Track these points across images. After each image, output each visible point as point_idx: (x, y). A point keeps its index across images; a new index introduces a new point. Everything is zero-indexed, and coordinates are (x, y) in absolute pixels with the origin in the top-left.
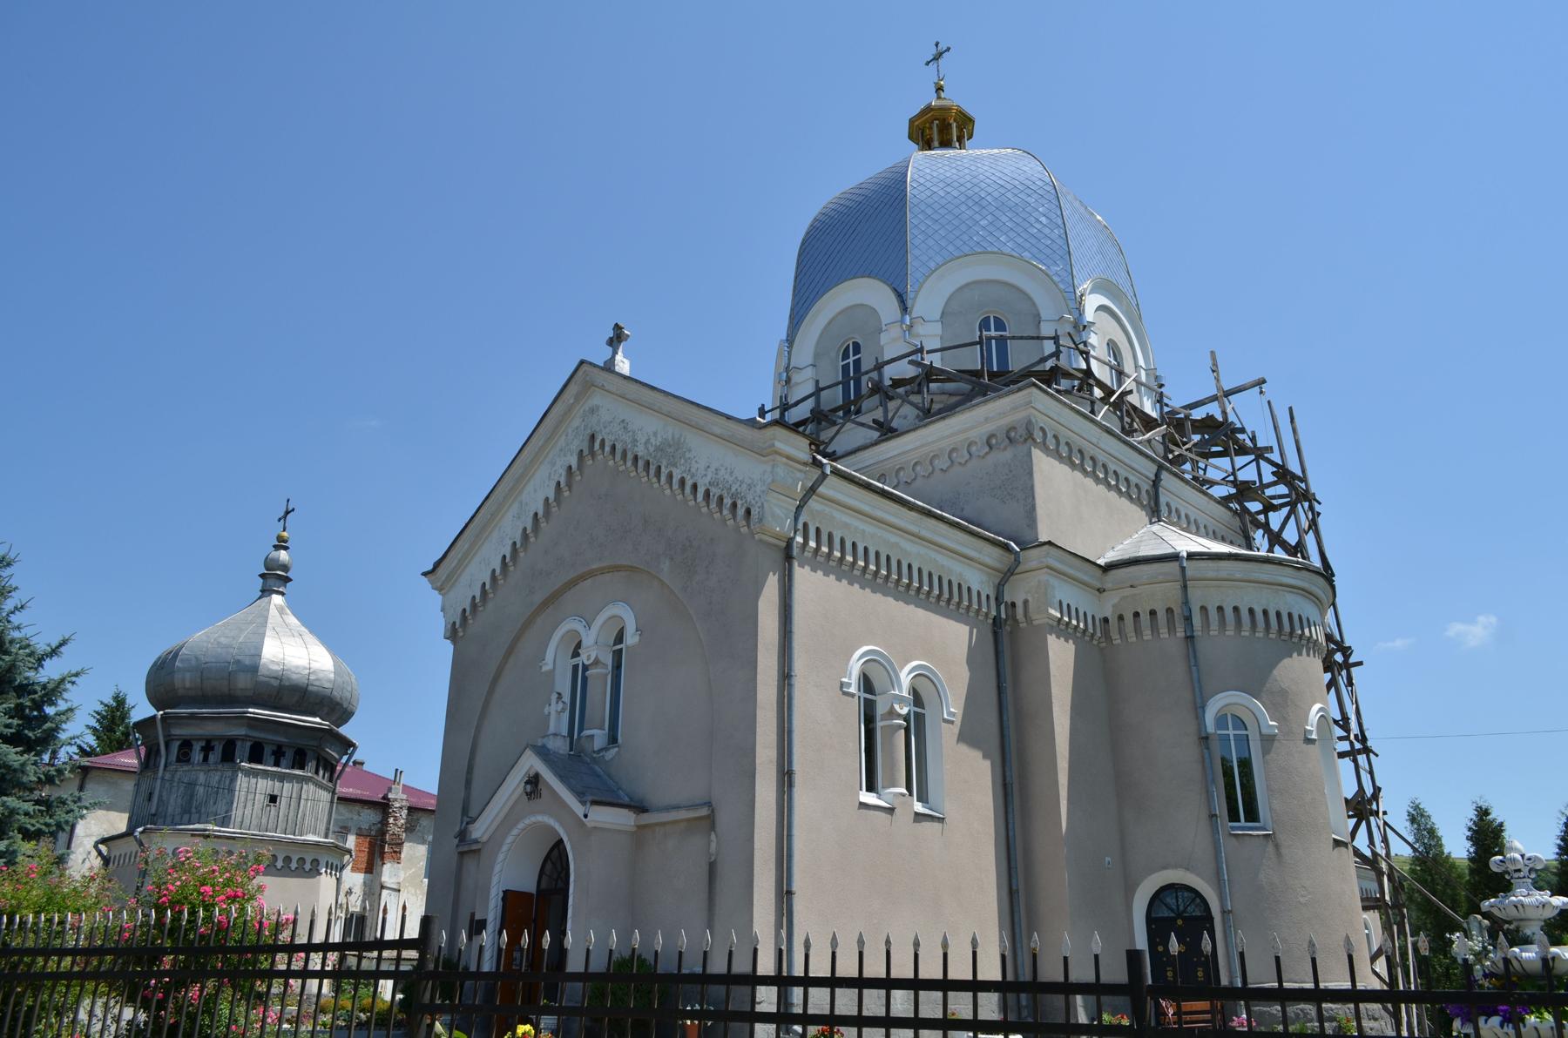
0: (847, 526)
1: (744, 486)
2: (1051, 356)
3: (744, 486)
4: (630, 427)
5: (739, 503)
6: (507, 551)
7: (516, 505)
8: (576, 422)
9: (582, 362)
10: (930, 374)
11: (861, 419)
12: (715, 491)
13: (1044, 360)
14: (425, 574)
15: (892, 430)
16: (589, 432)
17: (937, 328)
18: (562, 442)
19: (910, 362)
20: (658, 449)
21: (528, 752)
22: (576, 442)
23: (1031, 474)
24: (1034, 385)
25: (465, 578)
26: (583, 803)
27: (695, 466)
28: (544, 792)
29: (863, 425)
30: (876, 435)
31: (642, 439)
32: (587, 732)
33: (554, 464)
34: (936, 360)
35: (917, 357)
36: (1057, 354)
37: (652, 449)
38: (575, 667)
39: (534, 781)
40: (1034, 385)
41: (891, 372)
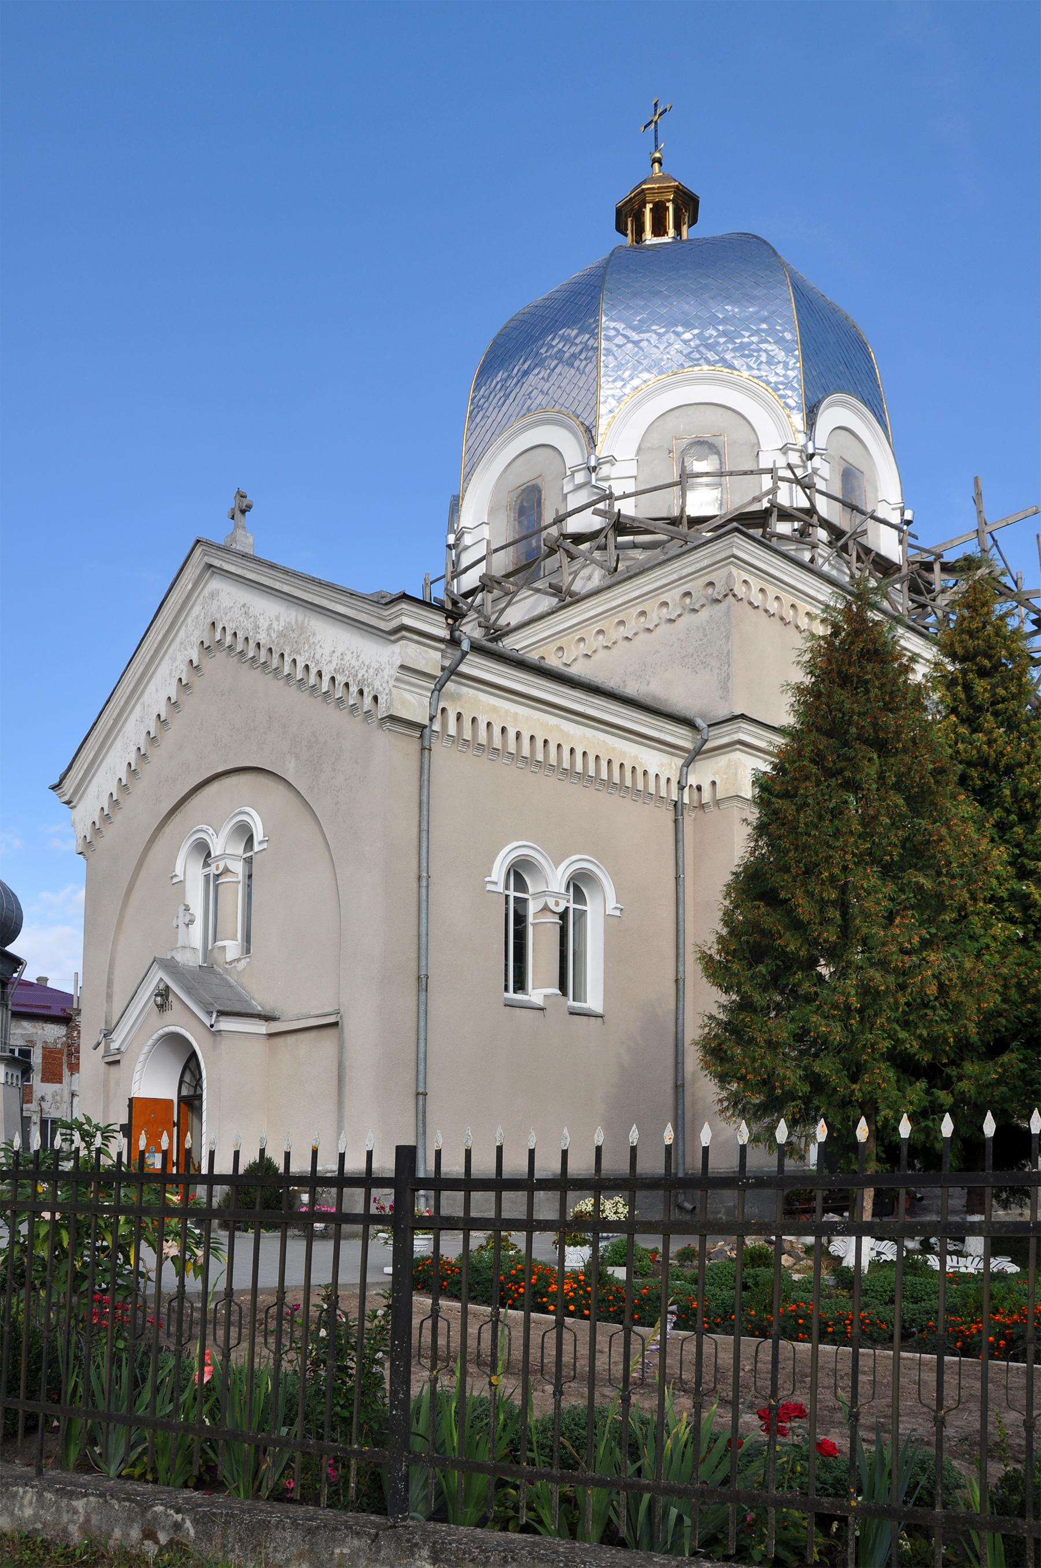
0: (495, 709)
1: (371, 671)
2: (767, 493)
3: (371, 671)
4: (251, 612)
5: (366, 690)
6: (132, 757)
7: (138, 707)
8: (197, 610)
9: (198, 541)
10: (620, 526)
11: (537, 585)
12: (340, 679)
13: (758, 499)
14: (53, 788)
15: (571, 594)
16: (209, 621)
17: (632, 469)
18: (182, 634)
19: (596, 512)
20: (281, 635)
21: (155, 967)
22: (197, 633)
23: (5, 1129)
24: (738, 749)
25: (93, 790)
26: (210, 1013)
27: (319, 651)
28: (175, 1004)
29: (538, 591)
30: (554, 601)
31: (264, 624)
32: (220, 943)
33: (174, 660)
34: (627, 508)
35: (601, 506)
36: (774, 491)
37: (274, 635)
38: (207, 877)
39: (164, 993)
40: (738, 749)
41: (573, 525)
